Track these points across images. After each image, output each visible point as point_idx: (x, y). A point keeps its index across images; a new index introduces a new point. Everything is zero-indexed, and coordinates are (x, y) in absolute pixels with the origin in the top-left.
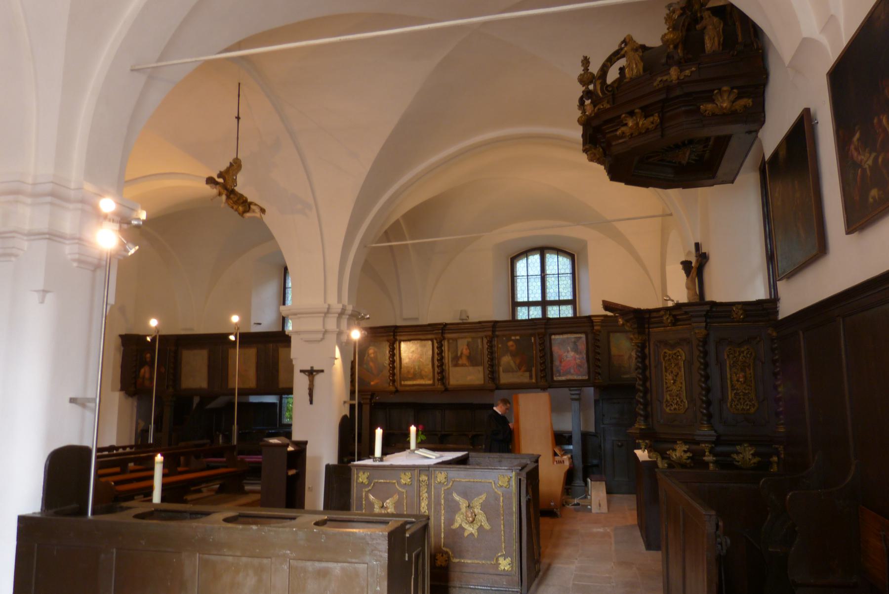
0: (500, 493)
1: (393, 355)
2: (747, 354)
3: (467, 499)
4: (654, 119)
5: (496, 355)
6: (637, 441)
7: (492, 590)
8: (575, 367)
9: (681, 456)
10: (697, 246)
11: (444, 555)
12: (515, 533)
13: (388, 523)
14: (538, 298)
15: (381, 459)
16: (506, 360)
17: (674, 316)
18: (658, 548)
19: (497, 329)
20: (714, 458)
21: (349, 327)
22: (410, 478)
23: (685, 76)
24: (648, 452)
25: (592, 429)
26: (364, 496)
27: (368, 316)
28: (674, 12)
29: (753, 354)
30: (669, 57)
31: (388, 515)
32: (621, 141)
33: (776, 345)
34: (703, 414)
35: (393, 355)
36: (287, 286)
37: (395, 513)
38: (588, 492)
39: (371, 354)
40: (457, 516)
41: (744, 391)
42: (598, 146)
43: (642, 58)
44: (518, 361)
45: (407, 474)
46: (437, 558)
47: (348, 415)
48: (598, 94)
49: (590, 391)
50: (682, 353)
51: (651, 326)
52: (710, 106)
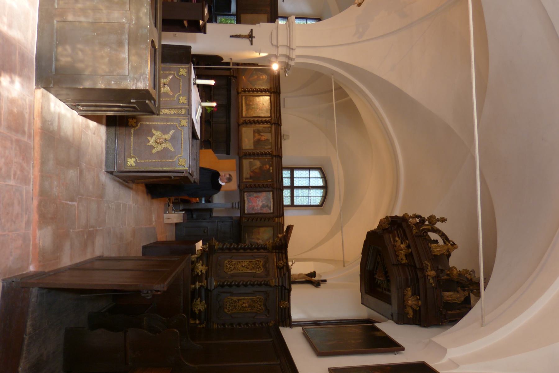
0: (175, 159)
1: (261, 91)
2: (259, 308)
3: (170, 139)
4: (404, 260)
5: (261, 157)
6: (207, 243)
7: (115, 154)
8: (253, 206)
9: (199, 269)
10: (325, 281)
11: (136, 124)
12: (150, 169)
13: (155, 89)
14: (296, 184)
15: (195, 84)
16: (257, 163)
17: (283, 268)
18: (144, 254)
19: (277, 158)
20: (197, 288)
21: (280, 63)
22: (183, 102)
23: (430, 280)
24: (201, 250)
25: (214, 215)
26: (171, 72)
27: (287, 76)
28: (470, 274)
29: (259, 312)
30: (442, 271)
31: (159, 88)
32: (392, 239)
33: (264, 325)
34: (223, 283)
35: (261, 91)
36: (308, 20)
37: (161, 92)
38: (176, 212)
39: (262, 77)
40: (160, 132)
41: (237, 306)
42: (389, 225)
43: (442, 254)
44: (256, 171)
45: (186, 101)
46: (134, 119)
47: (223, 61)
48: (422, 227)
49: (237, 214)
50: (260, 271)
51: (277, 254)
52: (410, 293)
